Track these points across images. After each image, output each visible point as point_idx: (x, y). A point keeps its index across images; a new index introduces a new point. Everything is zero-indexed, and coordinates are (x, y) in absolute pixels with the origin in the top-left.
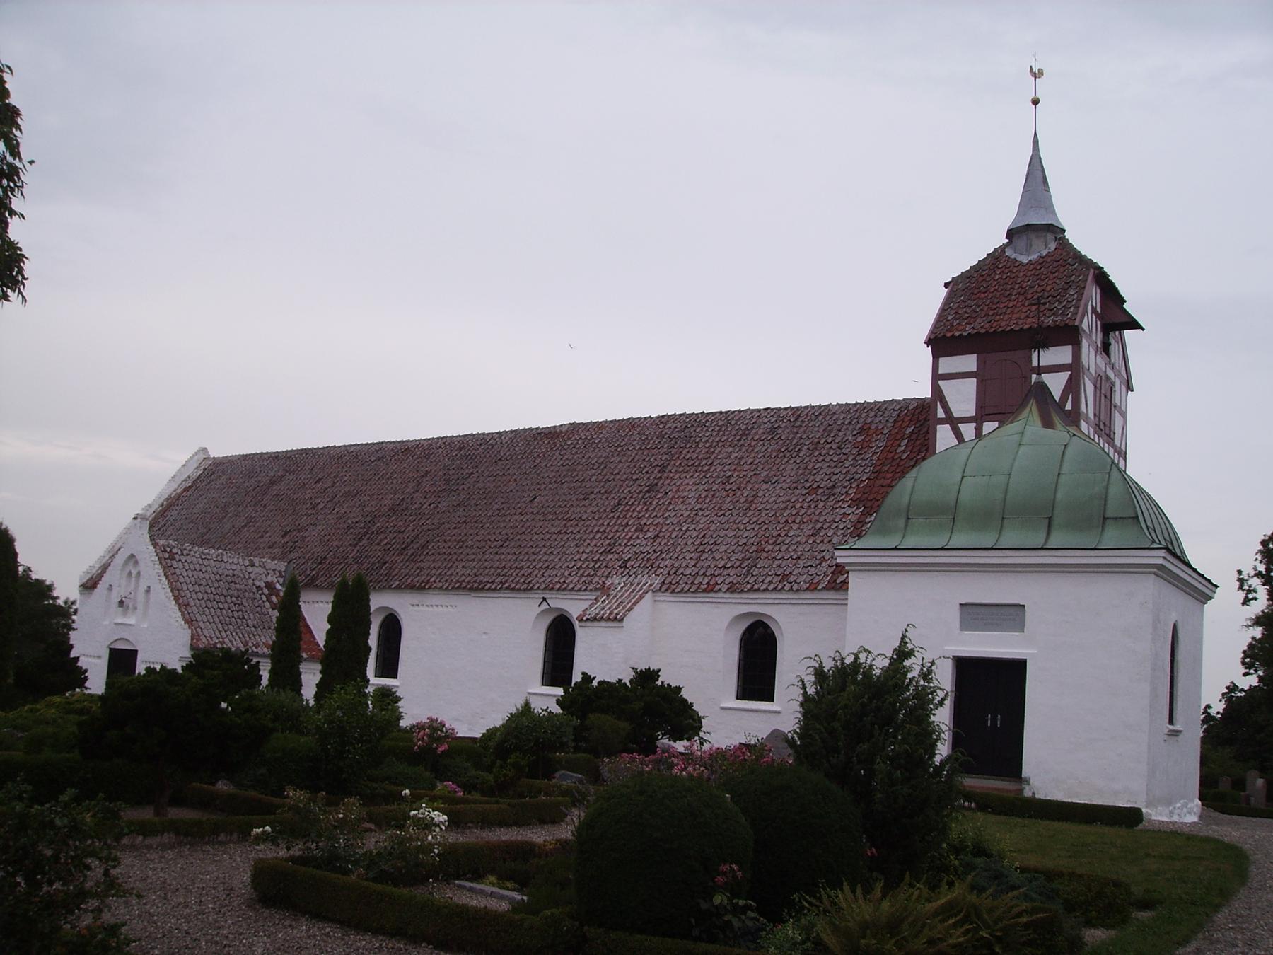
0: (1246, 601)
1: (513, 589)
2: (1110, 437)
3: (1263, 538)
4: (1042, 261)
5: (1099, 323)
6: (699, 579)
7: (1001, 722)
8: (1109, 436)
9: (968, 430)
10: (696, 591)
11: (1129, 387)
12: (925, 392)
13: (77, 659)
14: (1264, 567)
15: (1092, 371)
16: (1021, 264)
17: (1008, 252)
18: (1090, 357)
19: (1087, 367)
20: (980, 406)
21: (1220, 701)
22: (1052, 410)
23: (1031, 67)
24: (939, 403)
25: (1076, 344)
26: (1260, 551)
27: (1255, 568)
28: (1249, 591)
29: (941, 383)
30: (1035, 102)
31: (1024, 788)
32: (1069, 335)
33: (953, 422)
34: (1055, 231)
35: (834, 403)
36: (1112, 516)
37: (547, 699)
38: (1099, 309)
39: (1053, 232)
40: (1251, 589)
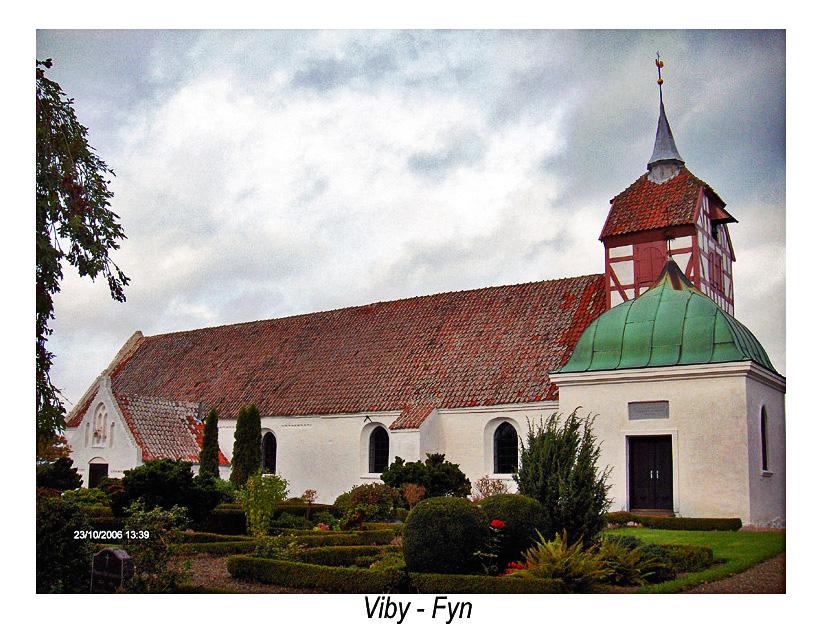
1: (347, 412)
2: (722, 294)
4: (670, 184)
6: (466, 398)
9: (630, 293)
10: (464, 406)
12: (602, 271)
13: (76, 469)
15: (706, 250)
18: (704, 242)
20: (636, 278)
25: (694, 234)
30: (660, 83)
32: (689, 229)
33: (621, 289)
34: (678, 164)
37: (376, 479)
39: (676, 164)
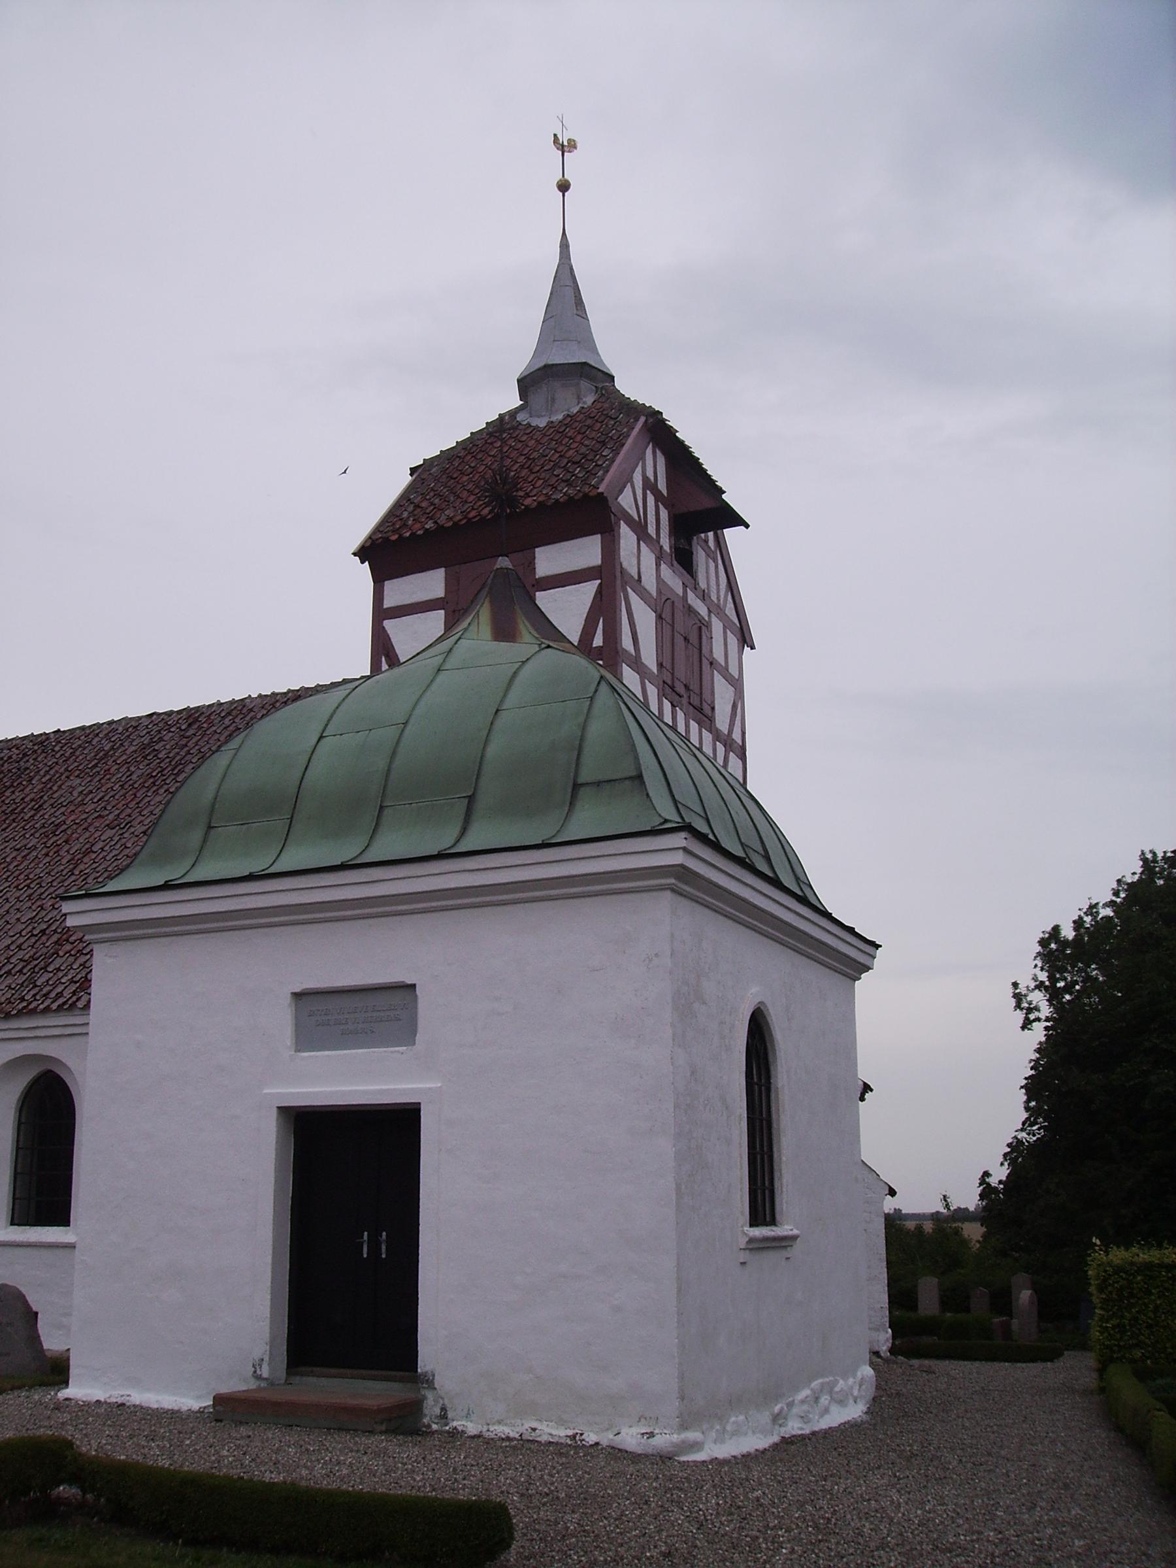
0: (1026, 1025)
2: (703, 714)
3: (1042, 935)
5: (664, 514)
7: (380, 1249)
8: (700, 710)
11: (745, 639)
14: (1046, 974)
16: (537, 428)
17: (520, 417)
19: (636, 577)
21: (1002, 1164)
22: (519, 611)
23: (555, 135)
24: (383, 659)
26: (1039, 954)
27: (1035, 979)
28: (1030, 1010)
29: (388, 624)
30: (564, 187)
31: (425, 1398)
34: (602, 379)
35: (254, 695)
36: (589, 780)
38: (662, 486)
39: (592, 379)
40: (1032, 1006)
